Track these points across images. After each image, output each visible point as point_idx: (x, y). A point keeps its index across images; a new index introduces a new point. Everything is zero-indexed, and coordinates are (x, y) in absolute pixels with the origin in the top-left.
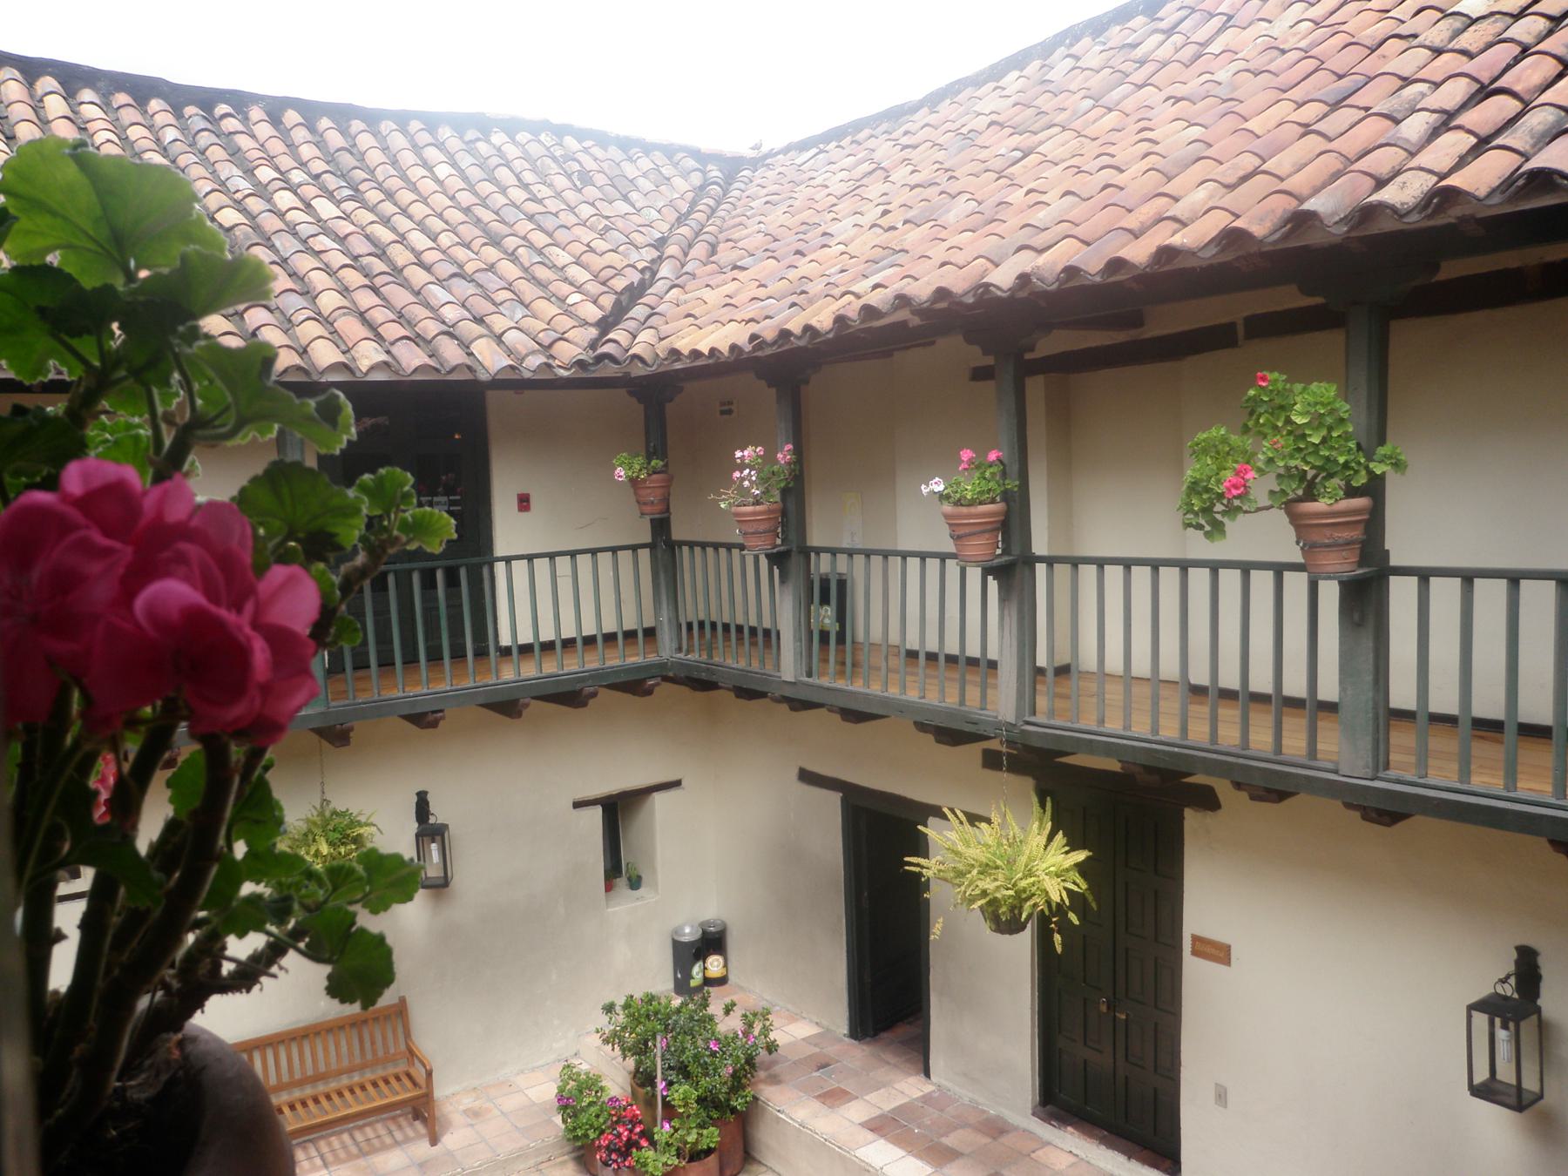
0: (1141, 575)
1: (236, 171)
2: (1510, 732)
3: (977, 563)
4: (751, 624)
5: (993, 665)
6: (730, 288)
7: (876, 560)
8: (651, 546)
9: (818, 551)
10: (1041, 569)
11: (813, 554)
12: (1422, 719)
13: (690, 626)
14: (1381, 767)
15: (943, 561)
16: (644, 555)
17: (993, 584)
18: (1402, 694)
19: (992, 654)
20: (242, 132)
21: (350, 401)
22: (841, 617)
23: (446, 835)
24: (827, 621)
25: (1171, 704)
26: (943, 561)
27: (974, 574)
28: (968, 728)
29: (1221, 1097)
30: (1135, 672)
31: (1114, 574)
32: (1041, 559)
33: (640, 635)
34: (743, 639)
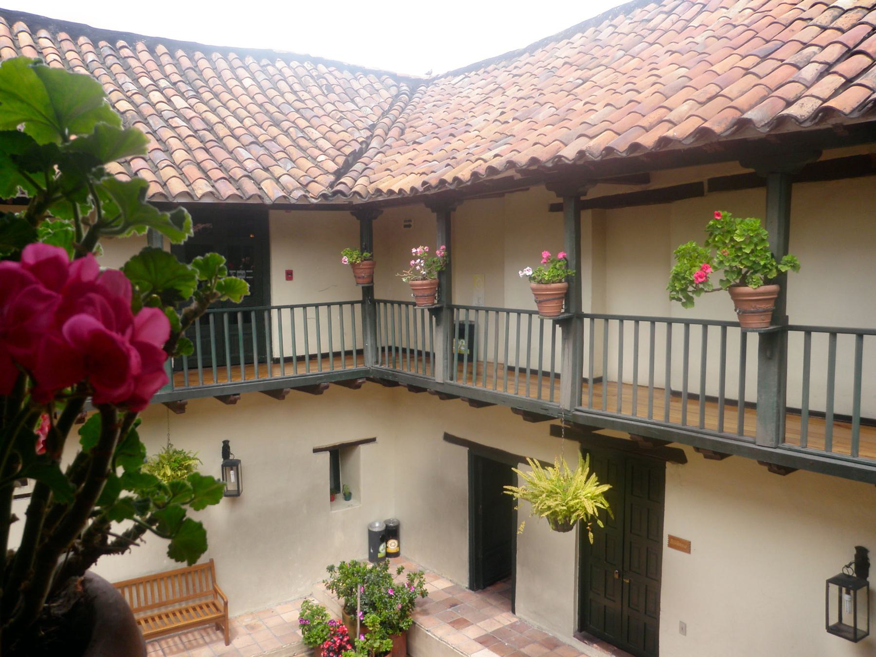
0: (645, 326)
3: (550, 317)
5: (558, 376)
7: (492, 314)
8: (362, 302)
9: (459, 308)
11: (455, 310)
15: (530, 315)
16: (358, 307)
17: (559, 329)
18: (794, 399)
19: (558, 370)
22: (471, 346)
24: (463, 348)
26: (530, 315)
27: (548, 324)
28: (542, 412)
29: (683, 629)
32: (587, 316)
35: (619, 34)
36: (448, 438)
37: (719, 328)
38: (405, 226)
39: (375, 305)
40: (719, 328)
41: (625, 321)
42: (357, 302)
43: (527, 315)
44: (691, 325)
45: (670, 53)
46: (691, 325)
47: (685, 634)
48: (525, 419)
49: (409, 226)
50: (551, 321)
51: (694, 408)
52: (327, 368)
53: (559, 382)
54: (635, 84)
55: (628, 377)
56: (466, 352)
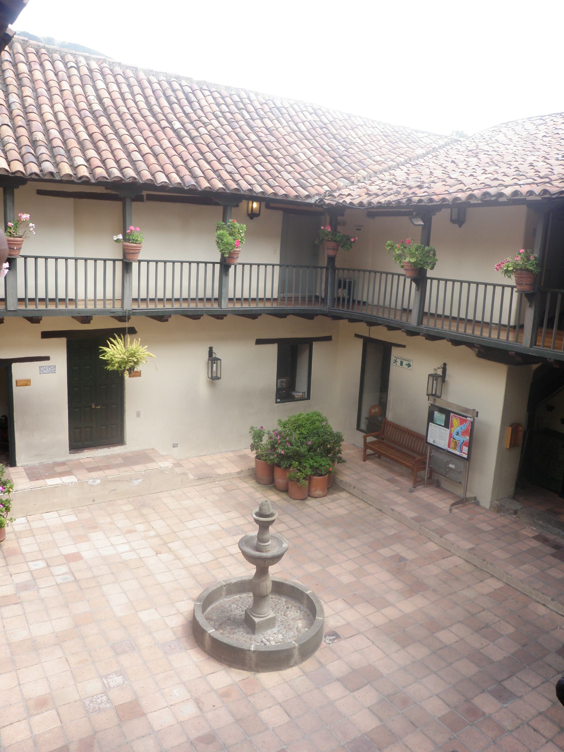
0: (262, 268)
1: (15, 83)
2: (450, 318)
3: (409, 277)
4: (364, 300)
5: (411, 311)
6: (457, 157)
7: (372, 274)
8: (327, 269)
9: (339, 269)
10: (429, 281)
11: (337, 271)
12: (450, 318)
13: (339, 299)
14: (533, 344)
15: (393, 275)
16: (277, 269)
17: (414, 285)
18: (426, 310)
19: (410, 308)
20: (23, 62)
21: (188, 189)
22: (349, 294)
23: (210, 376)
24: (345, 294)
25: (398, 314)
26: (393, 275)
27: (408, 281)
28: (441, 336)
30: (398, 308)
31: (384, 276)
32: (429, 278)
33: (293, 299)
34: (312, 300)
35: (548, 164)
36: (259, 342)
37: (452, 282)
38: (357, 229)
39: (335, 271)
40: (452, 282)
41: (433, 280)
42: (324, 268)
43: (437, 281)
44: (488, 286)
45: (504, 174)
46: (488, 286)
47: (137, 412)
48: (452, 344)
49: (360, 230)
50: (410, 279)
51: (446, 323)
52: (261, 306)
53: (411, 314)
54: (504, 181)
55: (393, 306)
56: (346, 297)
